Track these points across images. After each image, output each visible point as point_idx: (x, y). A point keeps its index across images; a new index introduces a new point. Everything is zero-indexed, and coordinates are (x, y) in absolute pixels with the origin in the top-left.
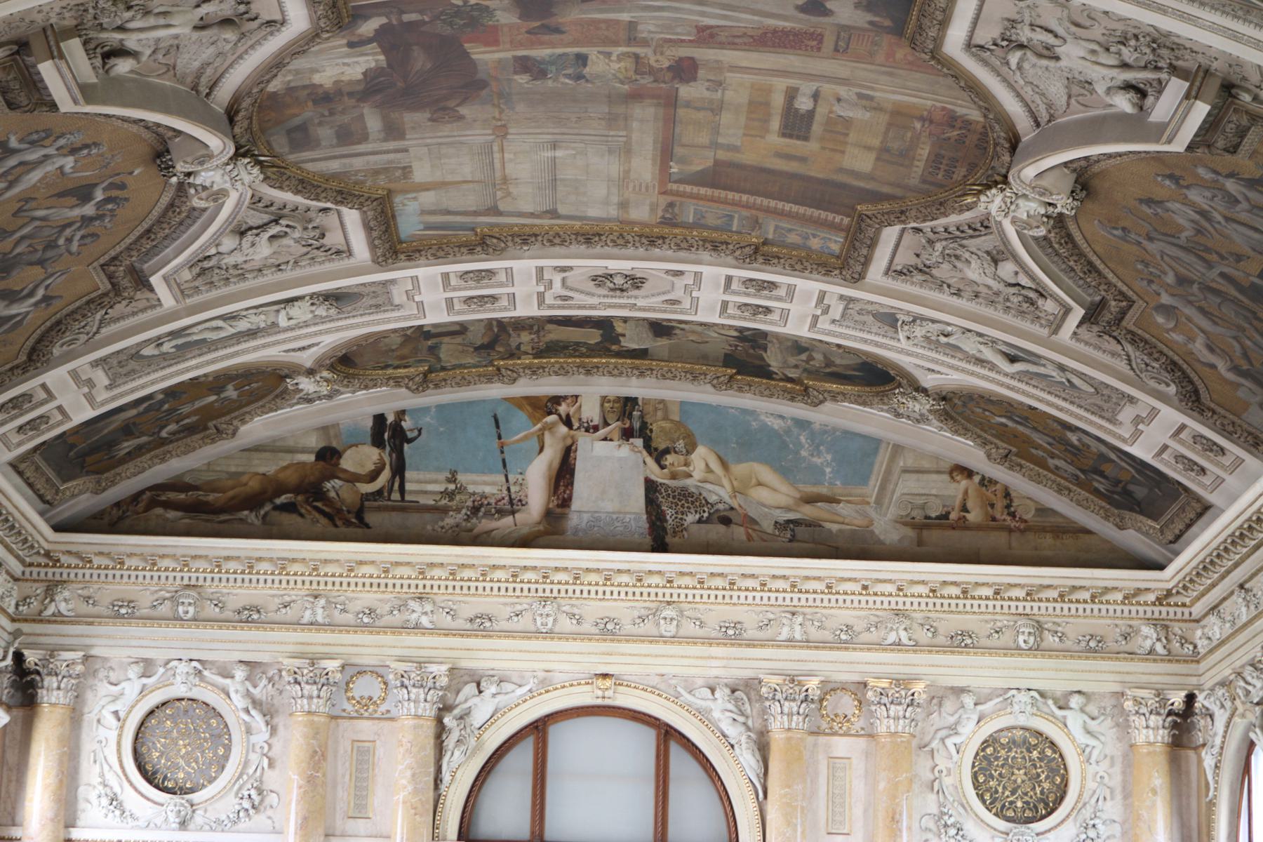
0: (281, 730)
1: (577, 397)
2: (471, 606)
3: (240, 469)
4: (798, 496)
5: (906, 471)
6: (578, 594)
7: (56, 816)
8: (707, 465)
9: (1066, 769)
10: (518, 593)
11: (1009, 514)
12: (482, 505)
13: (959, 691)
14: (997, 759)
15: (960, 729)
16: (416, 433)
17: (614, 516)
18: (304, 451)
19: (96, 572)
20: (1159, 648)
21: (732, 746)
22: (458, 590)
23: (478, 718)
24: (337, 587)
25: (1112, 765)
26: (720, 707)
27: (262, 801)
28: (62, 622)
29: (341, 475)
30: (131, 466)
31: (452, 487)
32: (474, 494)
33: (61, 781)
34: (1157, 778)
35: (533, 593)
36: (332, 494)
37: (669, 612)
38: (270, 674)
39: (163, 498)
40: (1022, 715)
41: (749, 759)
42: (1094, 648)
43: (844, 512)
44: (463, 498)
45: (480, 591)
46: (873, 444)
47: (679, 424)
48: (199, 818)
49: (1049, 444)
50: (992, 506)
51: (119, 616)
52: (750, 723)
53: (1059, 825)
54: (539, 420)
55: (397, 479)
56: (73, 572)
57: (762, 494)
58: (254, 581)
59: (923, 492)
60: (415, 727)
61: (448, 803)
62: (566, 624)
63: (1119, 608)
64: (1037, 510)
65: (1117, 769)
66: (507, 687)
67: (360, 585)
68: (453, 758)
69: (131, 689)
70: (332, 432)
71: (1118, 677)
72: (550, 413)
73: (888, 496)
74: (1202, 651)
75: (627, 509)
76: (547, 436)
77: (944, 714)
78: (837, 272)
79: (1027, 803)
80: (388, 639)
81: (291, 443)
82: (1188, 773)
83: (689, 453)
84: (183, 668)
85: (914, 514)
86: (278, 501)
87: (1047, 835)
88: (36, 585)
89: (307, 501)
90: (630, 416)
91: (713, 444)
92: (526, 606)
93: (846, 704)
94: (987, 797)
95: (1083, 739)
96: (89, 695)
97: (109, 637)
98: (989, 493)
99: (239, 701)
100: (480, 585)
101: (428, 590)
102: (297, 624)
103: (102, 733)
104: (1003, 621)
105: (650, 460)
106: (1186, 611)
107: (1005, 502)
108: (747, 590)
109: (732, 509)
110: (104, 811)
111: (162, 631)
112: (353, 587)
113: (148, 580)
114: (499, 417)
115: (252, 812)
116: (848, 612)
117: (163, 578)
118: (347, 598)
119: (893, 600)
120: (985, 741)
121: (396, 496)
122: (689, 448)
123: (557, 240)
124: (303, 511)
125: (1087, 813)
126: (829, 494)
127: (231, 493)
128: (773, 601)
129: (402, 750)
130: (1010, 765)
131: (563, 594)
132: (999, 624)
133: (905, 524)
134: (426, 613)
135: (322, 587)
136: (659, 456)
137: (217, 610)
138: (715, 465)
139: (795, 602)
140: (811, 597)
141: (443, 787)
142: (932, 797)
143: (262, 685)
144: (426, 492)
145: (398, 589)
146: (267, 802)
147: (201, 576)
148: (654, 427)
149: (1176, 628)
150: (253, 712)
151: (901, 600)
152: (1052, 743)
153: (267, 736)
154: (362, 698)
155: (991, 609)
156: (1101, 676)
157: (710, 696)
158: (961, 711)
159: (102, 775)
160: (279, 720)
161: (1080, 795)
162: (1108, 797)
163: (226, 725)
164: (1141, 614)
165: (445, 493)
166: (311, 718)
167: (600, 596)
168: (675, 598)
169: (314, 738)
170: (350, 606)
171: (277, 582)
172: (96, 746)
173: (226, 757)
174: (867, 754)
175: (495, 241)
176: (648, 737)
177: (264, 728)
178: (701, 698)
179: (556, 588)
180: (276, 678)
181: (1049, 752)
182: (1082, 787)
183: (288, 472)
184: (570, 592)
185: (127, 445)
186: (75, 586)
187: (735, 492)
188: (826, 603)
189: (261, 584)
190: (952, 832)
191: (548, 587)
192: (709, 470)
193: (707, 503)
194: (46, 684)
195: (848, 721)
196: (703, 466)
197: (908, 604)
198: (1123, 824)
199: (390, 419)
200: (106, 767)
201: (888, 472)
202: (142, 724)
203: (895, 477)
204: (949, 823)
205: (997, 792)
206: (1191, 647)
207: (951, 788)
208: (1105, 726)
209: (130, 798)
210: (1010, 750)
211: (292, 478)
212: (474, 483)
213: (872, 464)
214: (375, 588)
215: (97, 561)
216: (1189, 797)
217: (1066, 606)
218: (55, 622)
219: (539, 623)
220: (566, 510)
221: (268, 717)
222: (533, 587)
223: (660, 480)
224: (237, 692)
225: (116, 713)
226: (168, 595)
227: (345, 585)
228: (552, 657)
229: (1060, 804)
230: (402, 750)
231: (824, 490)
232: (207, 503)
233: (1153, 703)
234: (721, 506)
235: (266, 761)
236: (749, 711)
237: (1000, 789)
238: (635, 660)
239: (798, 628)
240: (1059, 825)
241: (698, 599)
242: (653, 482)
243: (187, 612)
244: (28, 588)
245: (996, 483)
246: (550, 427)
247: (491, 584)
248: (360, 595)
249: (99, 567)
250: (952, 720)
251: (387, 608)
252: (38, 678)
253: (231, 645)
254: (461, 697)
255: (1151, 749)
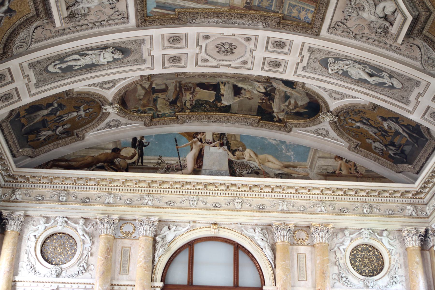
0: (96, 243)
1: (204, 133)
2: (167, 198)
3: (85, 155)
4: (282, 165)
5: (319, 158)
6: (205, 194)
7: (10, 270)
8: (250, 155)
9: (382, 258)
10: (184, 193)
11: (356, 172)
12: (170, 167)
13: (342, 230)
14: (358, 255)
15: (344, 243)
16: (147, 144)
17: (218, 171)
18: (108, 149)
19: (30, 185)
20: (414, 213)
21: (262, 249)
22: (162, 192)
23: (169, 238)
24: (118, 191)
25: (400, 256)
26: (258, 236)
27: (87, 268)
28: (17, 202)
29: (121, 157)
30: (45, 148)
31: (160, 161)
32: (168, 163)
33: (13, 258)
34: (418, 259)
35: (189, 194)
36: (117, 163)
37: (239, 200)
38: (92, 223)
39: (57, 164)
40: (366, 239)
41: (268, 252)
42: (391, 214)
43: (299, 171)
44: (164, 165)
45: (170, 193)
46: (307, 149)
47: (240, 142)
48: (64, 274)
49: (375, 133)
50: (350, 169)
51: (38, 200)
52: (268, 241)
53: (382, 277)
54: (191, 140)
55: (141, 158)
56: (22, 184)
57: (270, 165)
58: (88, 188)
59: (326, 164)
60: (146, 240)
61: (157, 269)
62: (201, 205)
63: (399, 199)
64: (366, 171)
65: (402, 257)
66: (179, 228)
67: (126, 190)
68: (160, 252)
69: (41, 227)
70: (118, 143)
71: (400, 224)
72: (195, 138)
73: (314, 166)
74: (429, 214)
75: (222, 169)
76: (194, 145)
77: (338, 239)
78: (310, 31)
79: (370, 271)
80: (136, 209)
81: (103, 146)
82: (427, 259)
83: (243, 151)
84: (60, 220)
85: (323, 171)
86: (98, 165)
87: (379, 281)
88: (8, 190)
89: (108, 165)
90: (223, 139)
91: (252, 148)
92: (187, 198)
93: (303, 235)
94: (355, 268)
95: (389, 247)
96: (26, 230)
97: (34, 207)
98: (349, 165)
99: (81, 232)
100: (170, 190)
101: (151, 192)
102: (103, 204)
103: (29, 243)
104: (359, 204)
105: (230, 153)
106: (422, 200)
107: (355, 168)
108: (267, 192)
109: (259, 169)
110: (29, 271)
111: (53, 204)
112: (124, 191)
113: (49, 188)
114: (177, 139)
115: (84, 271)
116: (302, 201)
117: (55, 187)
118: (122, 195)
119: (319, 196)
120: (353, 249)
121: (140, 164)
122: (244, 149)
123: (206, 16)
124: (107, 168)
125: (392, 273)
126: (293, 165)
127: (81, 162)
128: (276, 197)
129: (140, 248)
130: (363, 257)
131: (200, 194)
132: (357, 205)
133: (320, 175)
134: (150, 200)
135: (113, 191)
136: (233, 152)
137: (74, 198)
138: (253, 155)
139: (284, 197)
140: (289, 195)
141: (155, 263)
142: (336, 267)
143: (89, 227)
144: (151, 163)
145: (140, 192)
146: (89, 268)
147: (69, 186)
148: (231, 143)
149: (419, 207)
150: (86, 235)
151: (322, 196)
152: (377, 250)
153: (91, 244)
154: (126, 232)
155: (354, 200)
156: (394, 224)
157: (253, 232)
158: (344, 237)
159: (28, 258)
160: (95, 240)
161: (389, 267)
162: (399, 267)
163: (76, 242)
164: (407, 202)
165: (157, 163)
166: (107, 236)
167: (214, 194)
168: (241, 196)
169: (108, 243)
170: (122, 198)
171: (96, 188)
172: (27, 248)
173: (75, 253)
174: (311, 252)
175: (183, 15)
176: (229, 250)
177: (89, 242)
178: (250, 232)
179: (197, 191)
180: (95, 225)
181: (376, 253)
182: (390, 264)
183: (102, 156)
184: (203, 193)
185: (45, 134)
186: (23, 190)
187: (260, 164)
188: (295, 198)
189: (91, 189)
190: (344, 279)
191: (195, 191)
192: (250, 156)
193: (251, 167)
194: (10, 223)
195: (304, 241)
196: (248, 155)
197: (324, 198)
198: (405, 277)
199: (139, 139)
200: (30, 255)
201: (313, 158)
202: (45, 242)
203: (316, 160)
204: (343, 276)
205: (359, 267)
206: (425, 213)
207: (343, 264)
208: (396, 243)
209: (38, 266)
210: (362, 252)
211: (103, 158)
212: (168, 160)
213: (307, 156)
214: (132, 191)
215: (31, 180)
216: (428, 267)
217: (380, 199)
218: (14, 202)
219: (191, 204)
220: (200, 169)
221: (91, 238)
222: (189, 191)
223: (234, 160)
224: (80, 229)
225: (35, 236)
226: (56, 193)
227: (121, 190)
228: (196, 216)
229: (381, 271)
230: (140, 248)
231: (291, 163)
232: (72, 165)
233: (413, 231)
234: (255, 168)
235: (90, 253)
236: (268, 237)
237: (360, 266)
238: (226, 217)
239: (285, 206)
240: (382, 277)
241: (249, 196)
242: (231, 160)
243: (63, 199)
244: (6, 190)
245: (351, 162)
246: (195, 142)
247: (174, 190)
248: (126, 194)
249: (32, 183)
250: (341, 240)
251: (136, 198)
252: (7, 221)
253: (78, 211)
254: (162, 232)
255: (414, 248)
